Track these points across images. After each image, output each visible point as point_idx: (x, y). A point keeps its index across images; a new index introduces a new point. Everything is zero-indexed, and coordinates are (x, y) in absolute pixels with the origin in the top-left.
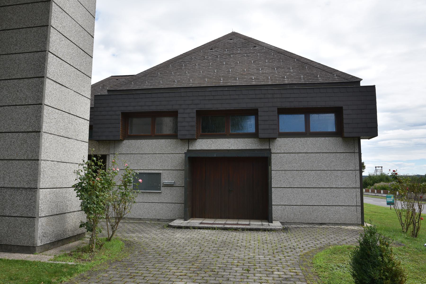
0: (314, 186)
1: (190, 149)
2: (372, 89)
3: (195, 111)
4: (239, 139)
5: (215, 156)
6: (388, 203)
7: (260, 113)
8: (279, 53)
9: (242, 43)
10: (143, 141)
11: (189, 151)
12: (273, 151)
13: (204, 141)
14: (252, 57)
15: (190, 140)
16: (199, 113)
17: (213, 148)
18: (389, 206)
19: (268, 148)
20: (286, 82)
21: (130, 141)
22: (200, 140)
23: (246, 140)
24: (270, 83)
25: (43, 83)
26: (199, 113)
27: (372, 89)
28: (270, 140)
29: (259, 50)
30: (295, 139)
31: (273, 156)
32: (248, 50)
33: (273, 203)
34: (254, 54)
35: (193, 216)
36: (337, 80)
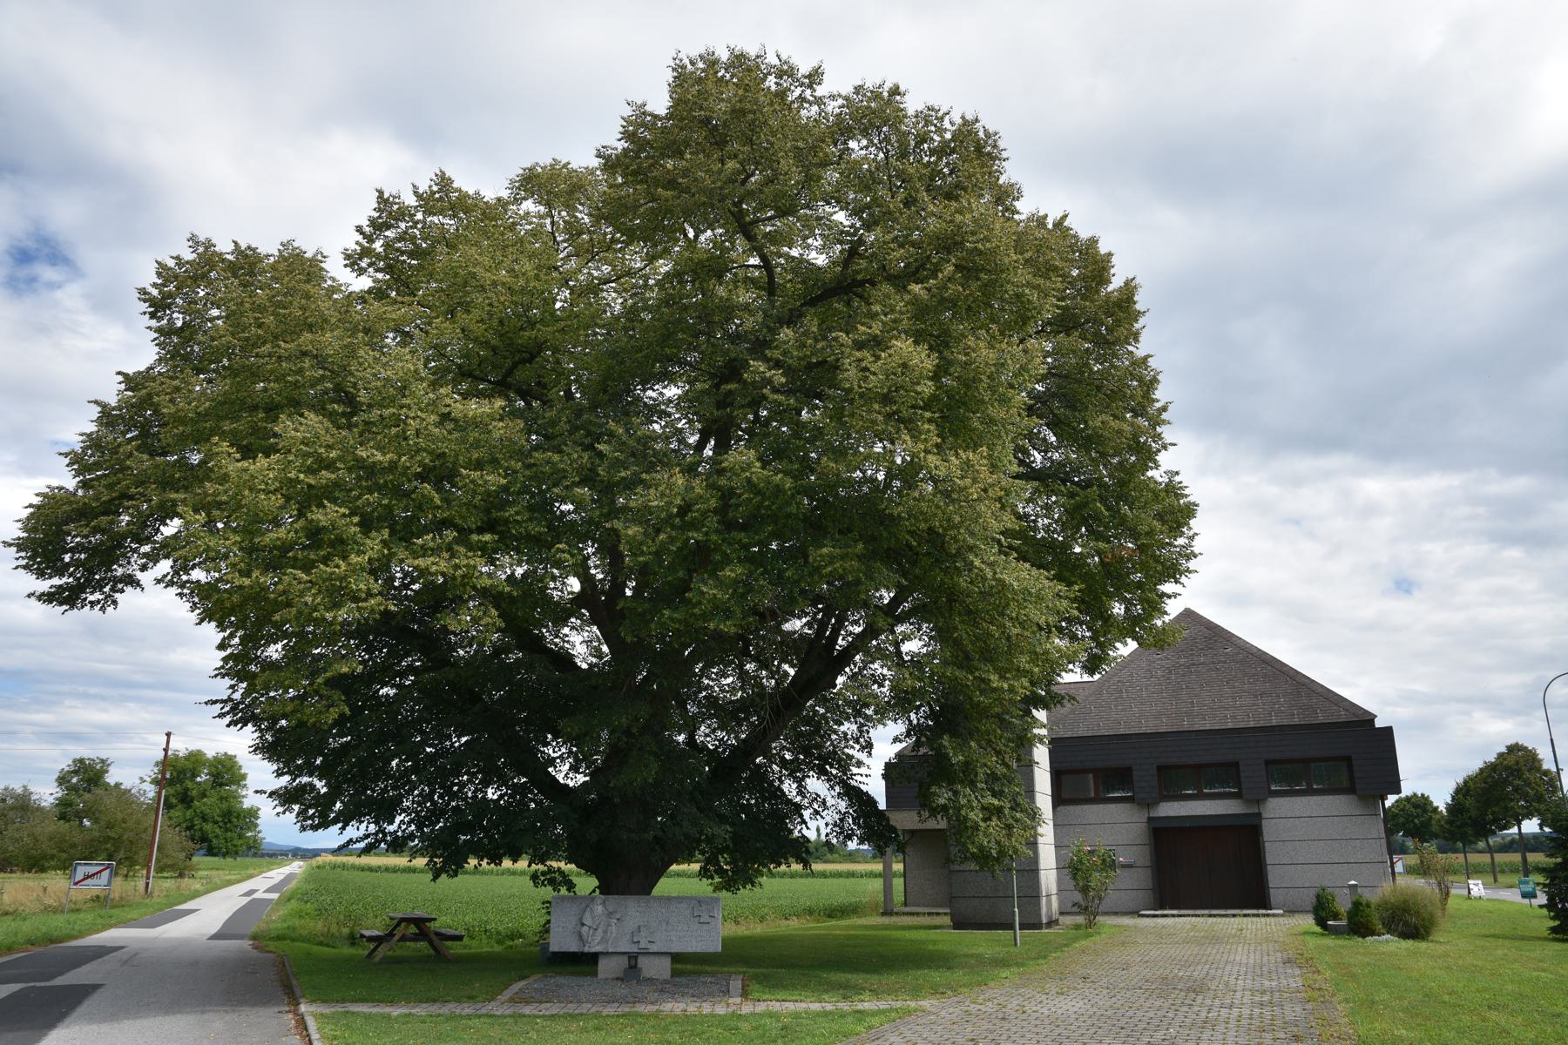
0: (1326, 860)
1: (1151, 815)
2: (1388, 731)
3: (1155, 767)
4: (1217, 802)
5: (1188, 825)
6: (1524, 895)
7: (1241, 768)
8: (1264, 661)
9: (1206, 637)
10: (1085, 807)
11: (1150, 819)
12: (1264, 816)
13: (1169, 804)
14: (1224, 672)
15: (1150, 804)
16: (1160, 768)
17: (1183, 813)
18: (1526, 901)
19: (1257, 811)
20: (1274, 723)
21: (1067, 807)
22: (1164, 804)
23: (1226, 802)
24: (1252, 724)
25: (1032, 772)
26: (1160, 768)
27: (1388, 731)
28: (1259, 801)
29: (1233, 656)
30: (1293, 799)
31: (1264, 822)
32: (1216, 655)
33: (1271, 886)
34: (1226, 665)
35: (1162, 908)
36: (1343, 716)
